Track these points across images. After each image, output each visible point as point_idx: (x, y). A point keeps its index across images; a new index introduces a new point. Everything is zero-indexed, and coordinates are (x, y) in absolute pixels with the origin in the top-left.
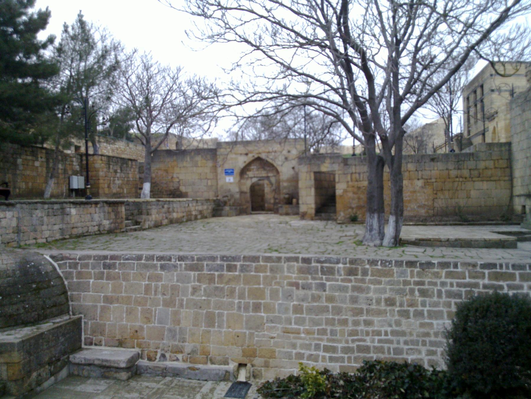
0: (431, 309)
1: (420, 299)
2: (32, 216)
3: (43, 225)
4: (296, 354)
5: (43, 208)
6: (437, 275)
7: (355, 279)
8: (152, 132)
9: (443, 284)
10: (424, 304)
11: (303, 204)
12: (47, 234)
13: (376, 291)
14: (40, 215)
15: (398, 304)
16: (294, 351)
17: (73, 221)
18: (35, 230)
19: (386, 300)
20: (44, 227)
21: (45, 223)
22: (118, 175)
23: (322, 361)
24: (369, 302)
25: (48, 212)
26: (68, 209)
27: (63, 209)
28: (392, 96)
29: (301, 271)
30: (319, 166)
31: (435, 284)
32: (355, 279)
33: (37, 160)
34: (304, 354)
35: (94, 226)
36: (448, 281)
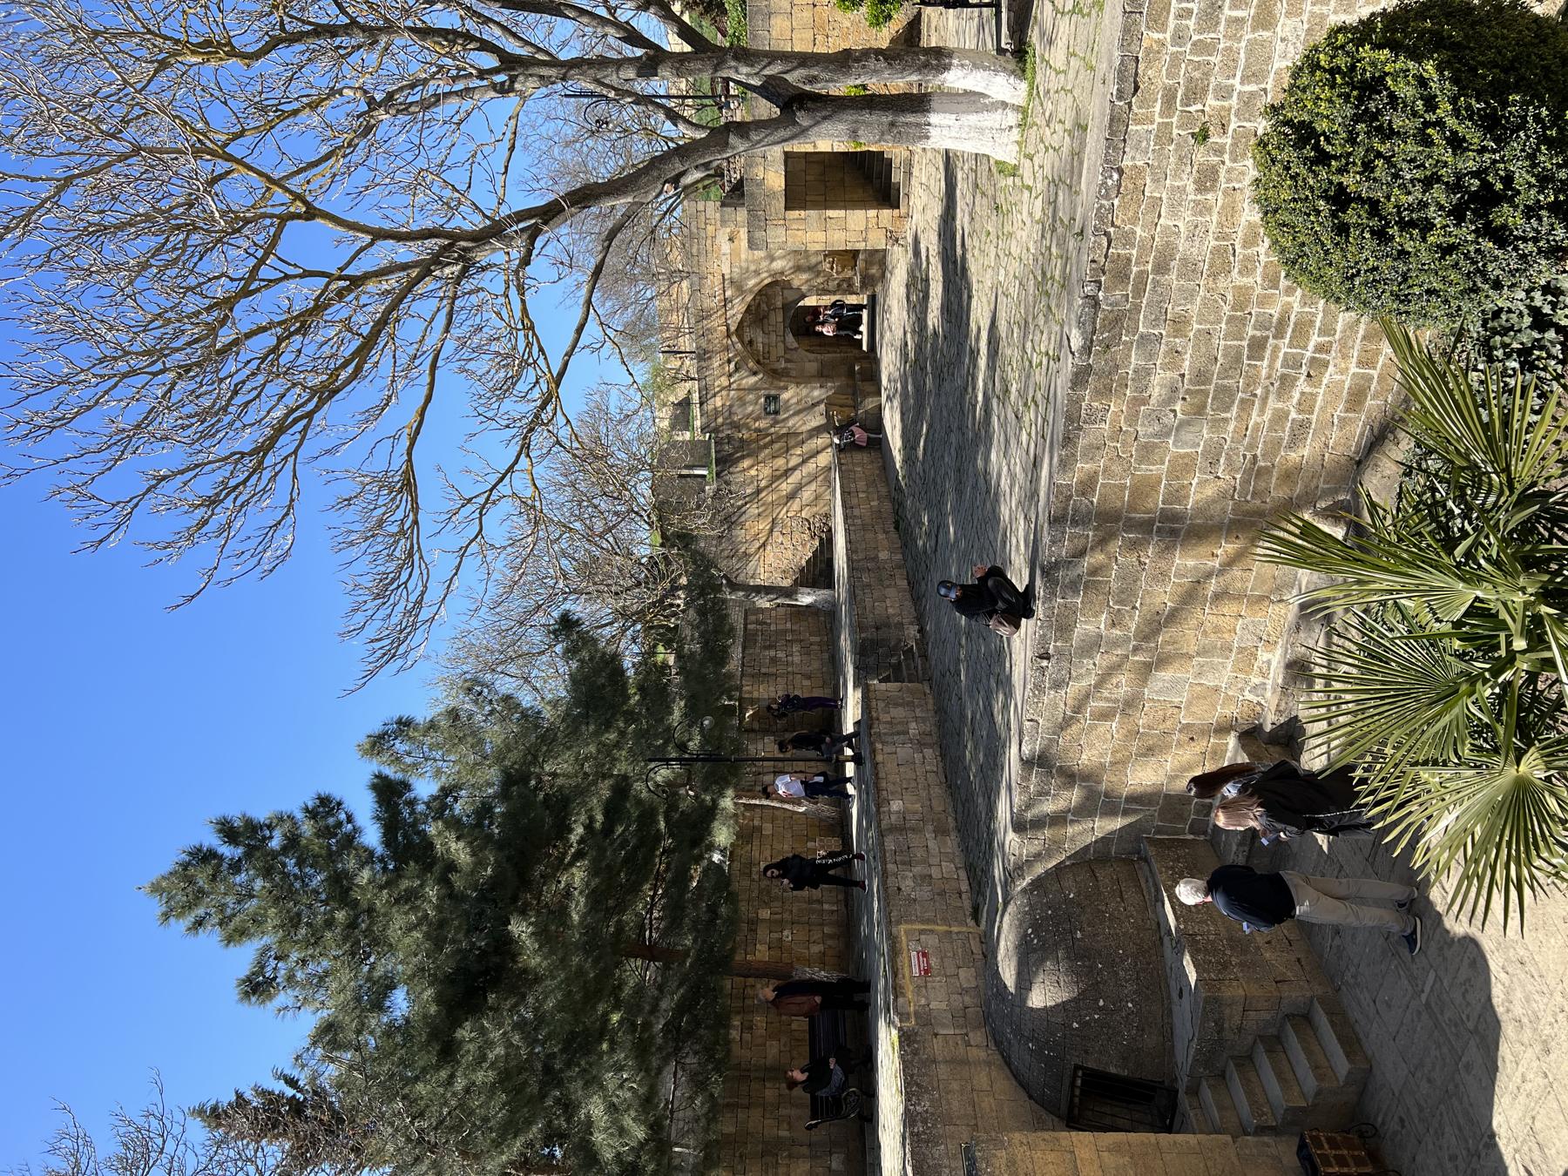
0: (1239, 74)
1: (1211, 101)
2: (915, 900)
3: (930, 876)
4: (1300, 412)
5: (896, 875)
6: (1154, 54)
7: (1137, 264)
8: (1030, 1004)
9: (1179, 38)
10: (1224, 93)
11: (865, 240)
12: (948, 867)
13: (1174, 209)
14: (909, 882)
15: (1215, 159)
16: (1293, 415)
17: (918, 806)
18: (942, 893)
19: (1201, 188)
20: (935, 872)
21: (925, 872)
22: (781, 654)
23: (1328, 352)
24: (1200, 231)
25: (904, 863)
26: (893, 818)
27: (893, 829)
28: (898, 457)
29: (1105, 392)
30: (771, 195)
31: (1176, 60)
32: (1137, 264)
33: (760, 829)
34: (1303, 393)
35: (924, 757)
36: (1172, 23)
